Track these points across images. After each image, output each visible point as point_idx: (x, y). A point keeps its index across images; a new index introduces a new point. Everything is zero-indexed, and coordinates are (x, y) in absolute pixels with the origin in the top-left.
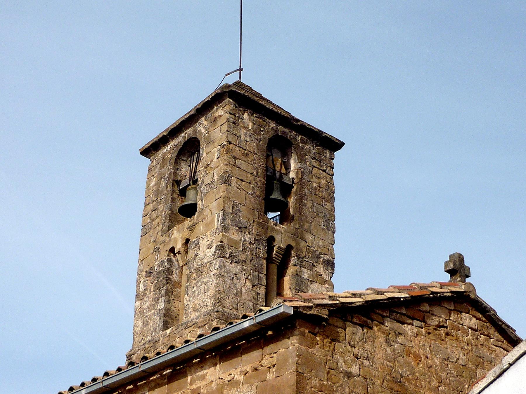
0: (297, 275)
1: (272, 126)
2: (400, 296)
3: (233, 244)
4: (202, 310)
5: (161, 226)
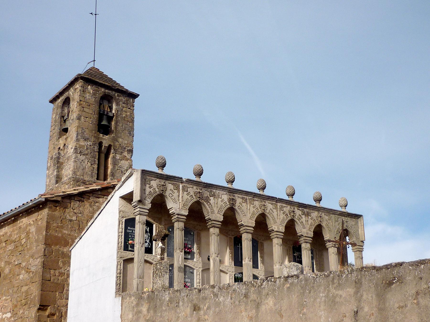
0: (114, 157)
1: (102, 90)
2: (96, 188)
3: (81, 147)
4: (69, 177)
5: (56, 137)
